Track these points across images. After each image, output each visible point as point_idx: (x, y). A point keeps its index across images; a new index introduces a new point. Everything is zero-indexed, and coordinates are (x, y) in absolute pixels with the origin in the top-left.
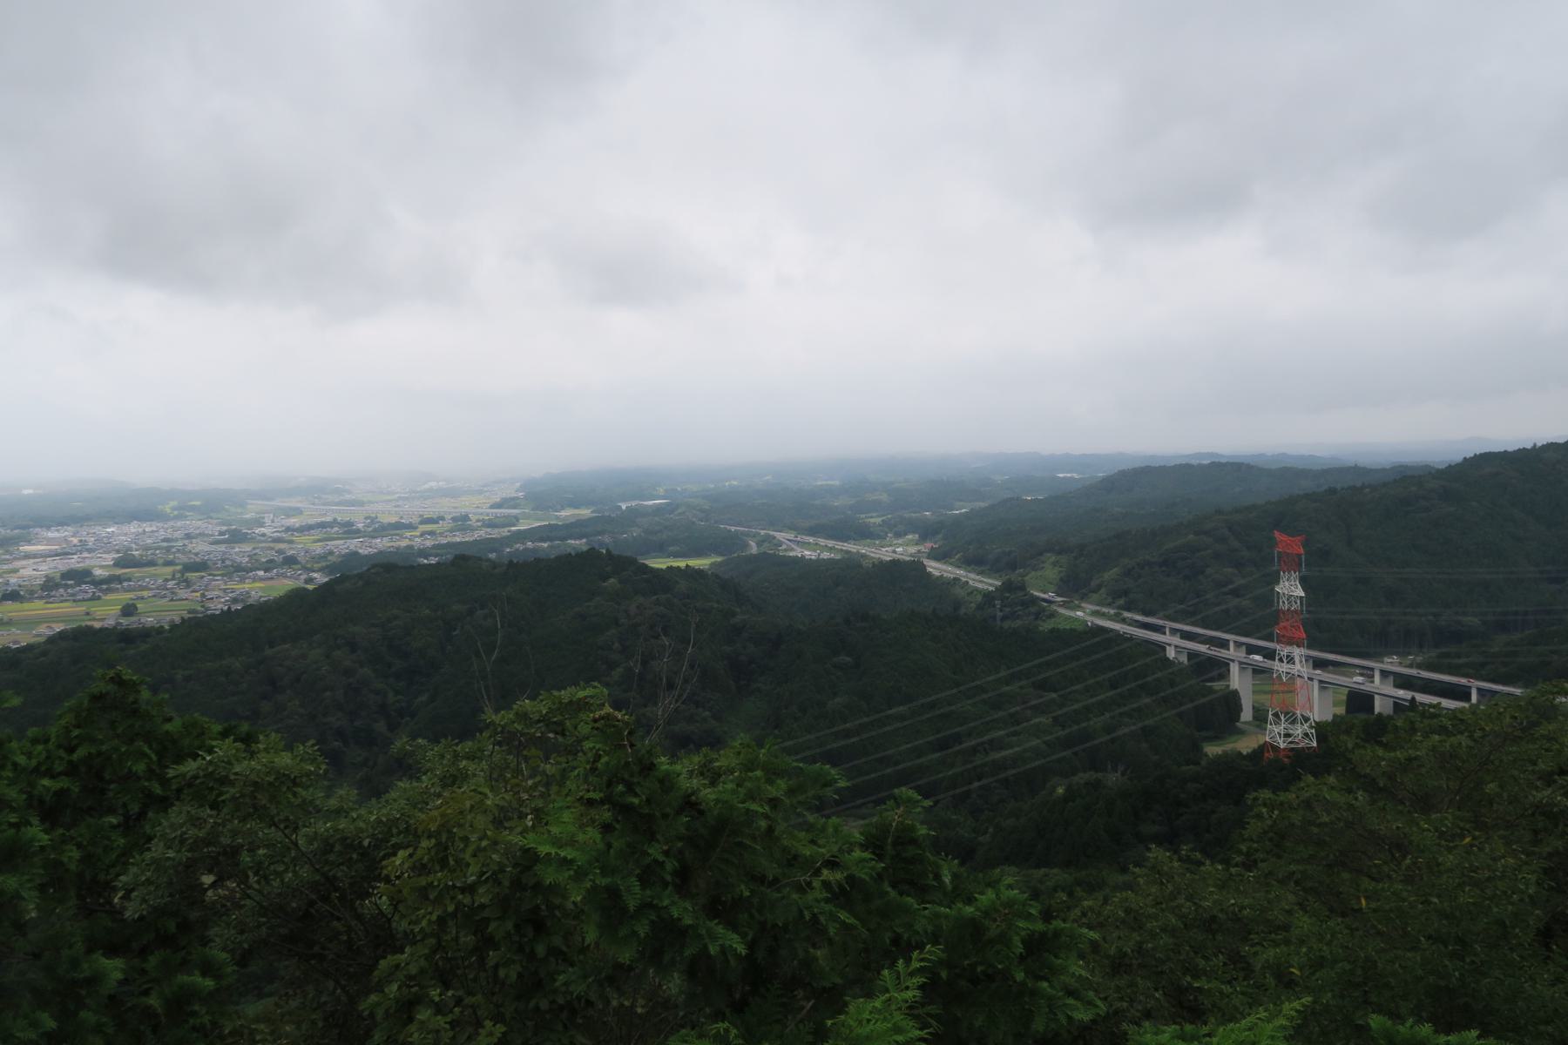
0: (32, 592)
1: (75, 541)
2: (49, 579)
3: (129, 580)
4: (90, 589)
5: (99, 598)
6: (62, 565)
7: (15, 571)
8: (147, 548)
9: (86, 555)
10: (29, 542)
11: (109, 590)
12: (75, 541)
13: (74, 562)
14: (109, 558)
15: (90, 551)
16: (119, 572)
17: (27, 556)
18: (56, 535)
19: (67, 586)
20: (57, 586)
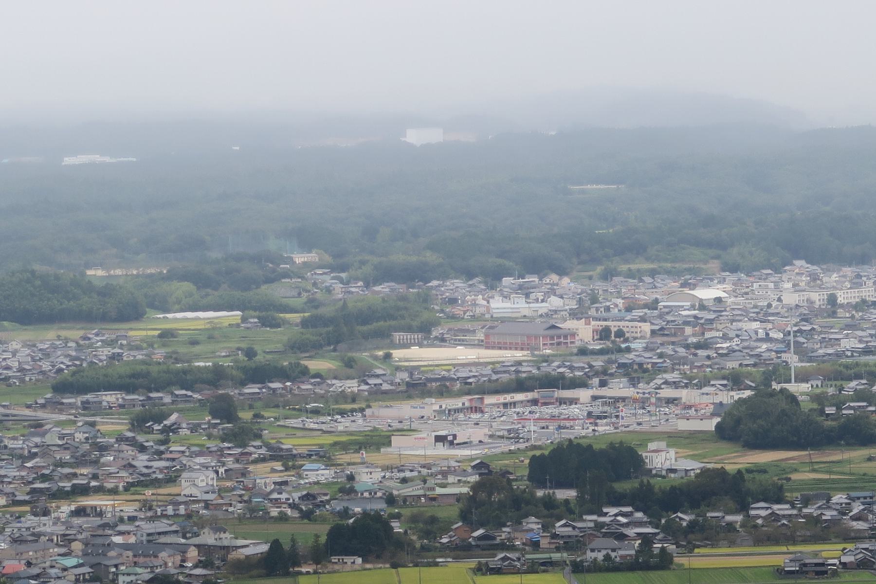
0: (431, 527)
1: (584, 332)
2: (490, 479)
3: (776, 495)
4: (636, 525)
5: (664, 562)
6: (539, 426)
7: (376, 441)
8: (840, 374)
9: (619, 388)
10: (425, 331)
11: (702, 534)
12: (584, 332)
13: (577, 418)
14: (704, 406)
15: (636, 373)
16: (737, 460)
17: (418, 386)
18: (519, 306)
19: (550, 510)
20: (519, 506)
